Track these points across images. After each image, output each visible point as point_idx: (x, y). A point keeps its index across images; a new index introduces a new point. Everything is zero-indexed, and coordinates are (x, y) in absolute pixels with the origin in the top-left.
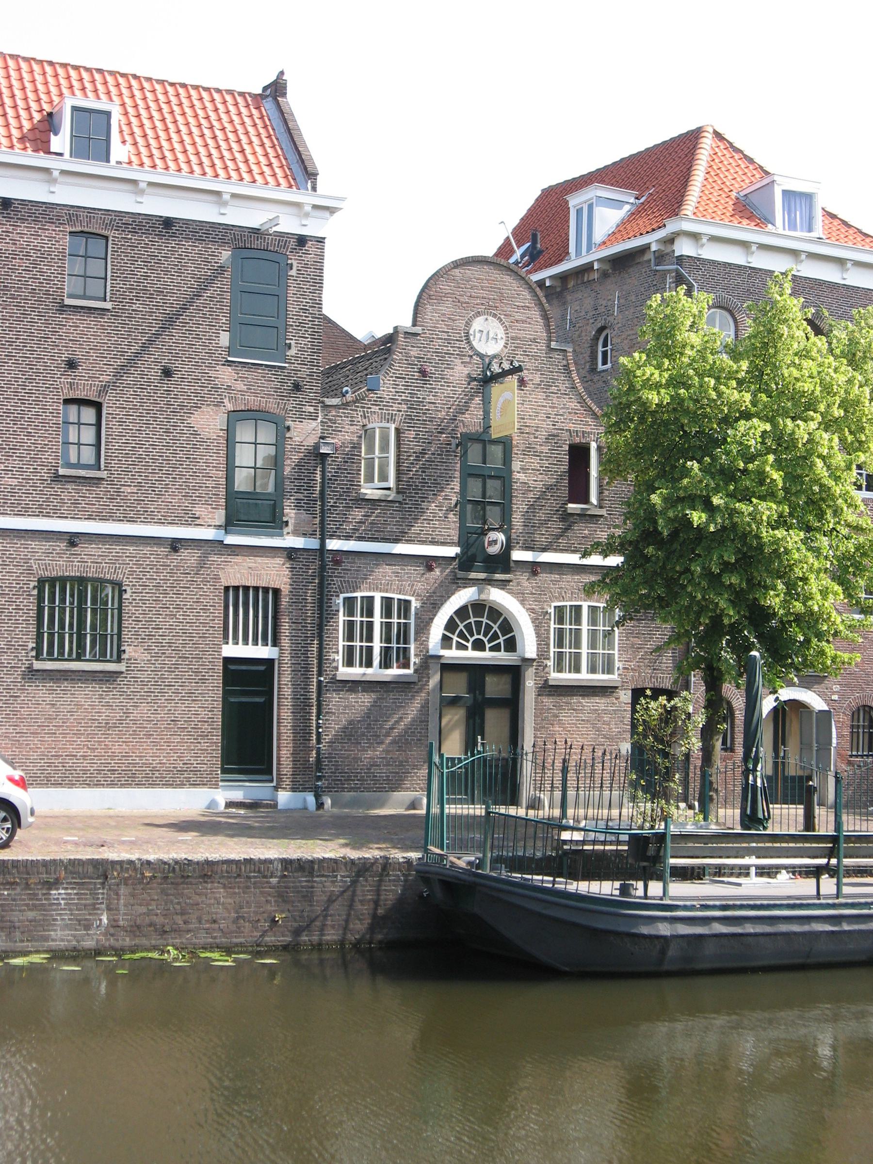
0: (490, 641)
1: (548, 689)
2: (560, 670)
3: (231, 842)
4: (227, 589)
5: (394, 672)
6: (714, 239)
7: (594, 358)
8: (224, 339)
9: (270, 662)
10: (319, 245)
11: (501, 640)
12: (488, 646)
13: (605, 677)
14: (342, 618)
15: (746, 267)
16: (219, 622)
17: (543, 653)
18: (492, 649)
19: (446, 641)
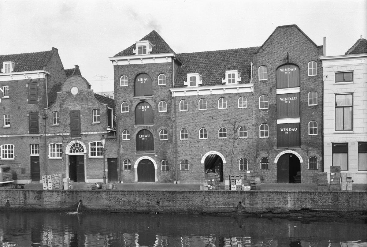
0: (79, 150)
1: (88, 159)
2: (51, 157)
3: (135, 175)
4: (30, 144)
5: (11, 158)
6: (118, 60)
7: (257, 133)
8: (28, 100)
9: (38, 157)
10: (333, 152)
11: (82, 150)
12: (79, 151)
13: (6, 158)
14: (50, 148)
15: (129, 65)
16: (29, 151)
17: (88, 153)
18: (80, 152)
19: (71, 151)
